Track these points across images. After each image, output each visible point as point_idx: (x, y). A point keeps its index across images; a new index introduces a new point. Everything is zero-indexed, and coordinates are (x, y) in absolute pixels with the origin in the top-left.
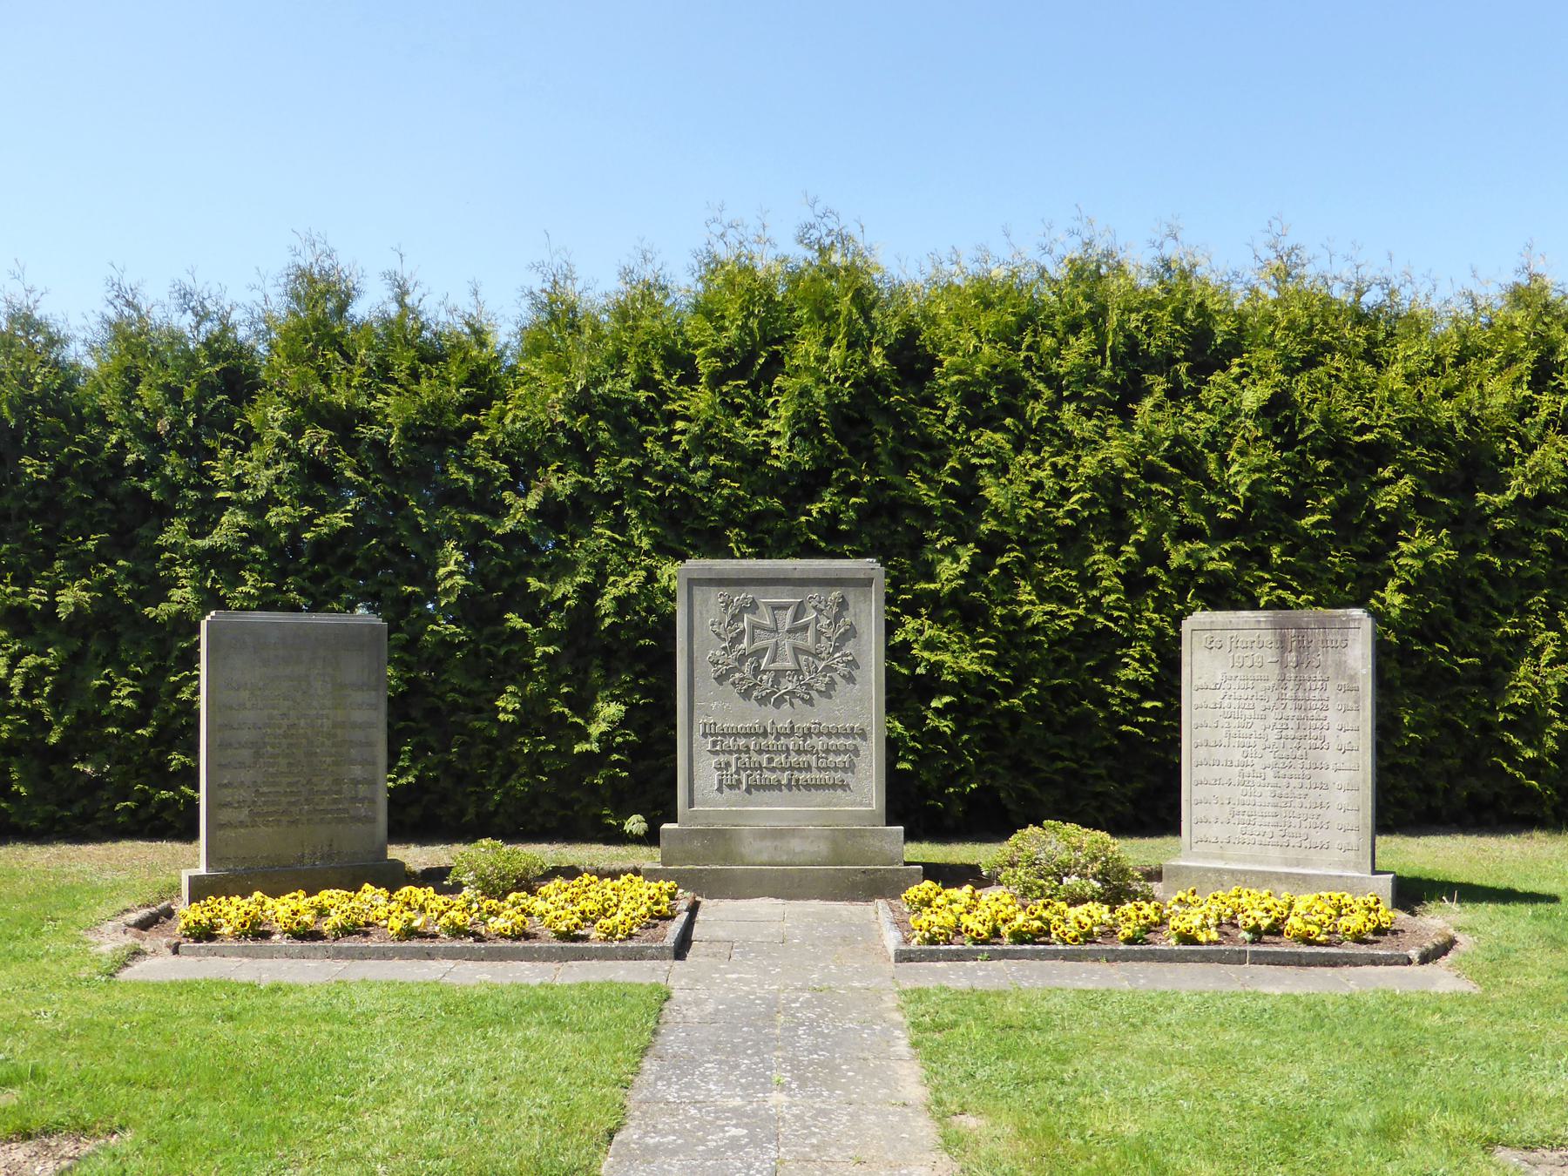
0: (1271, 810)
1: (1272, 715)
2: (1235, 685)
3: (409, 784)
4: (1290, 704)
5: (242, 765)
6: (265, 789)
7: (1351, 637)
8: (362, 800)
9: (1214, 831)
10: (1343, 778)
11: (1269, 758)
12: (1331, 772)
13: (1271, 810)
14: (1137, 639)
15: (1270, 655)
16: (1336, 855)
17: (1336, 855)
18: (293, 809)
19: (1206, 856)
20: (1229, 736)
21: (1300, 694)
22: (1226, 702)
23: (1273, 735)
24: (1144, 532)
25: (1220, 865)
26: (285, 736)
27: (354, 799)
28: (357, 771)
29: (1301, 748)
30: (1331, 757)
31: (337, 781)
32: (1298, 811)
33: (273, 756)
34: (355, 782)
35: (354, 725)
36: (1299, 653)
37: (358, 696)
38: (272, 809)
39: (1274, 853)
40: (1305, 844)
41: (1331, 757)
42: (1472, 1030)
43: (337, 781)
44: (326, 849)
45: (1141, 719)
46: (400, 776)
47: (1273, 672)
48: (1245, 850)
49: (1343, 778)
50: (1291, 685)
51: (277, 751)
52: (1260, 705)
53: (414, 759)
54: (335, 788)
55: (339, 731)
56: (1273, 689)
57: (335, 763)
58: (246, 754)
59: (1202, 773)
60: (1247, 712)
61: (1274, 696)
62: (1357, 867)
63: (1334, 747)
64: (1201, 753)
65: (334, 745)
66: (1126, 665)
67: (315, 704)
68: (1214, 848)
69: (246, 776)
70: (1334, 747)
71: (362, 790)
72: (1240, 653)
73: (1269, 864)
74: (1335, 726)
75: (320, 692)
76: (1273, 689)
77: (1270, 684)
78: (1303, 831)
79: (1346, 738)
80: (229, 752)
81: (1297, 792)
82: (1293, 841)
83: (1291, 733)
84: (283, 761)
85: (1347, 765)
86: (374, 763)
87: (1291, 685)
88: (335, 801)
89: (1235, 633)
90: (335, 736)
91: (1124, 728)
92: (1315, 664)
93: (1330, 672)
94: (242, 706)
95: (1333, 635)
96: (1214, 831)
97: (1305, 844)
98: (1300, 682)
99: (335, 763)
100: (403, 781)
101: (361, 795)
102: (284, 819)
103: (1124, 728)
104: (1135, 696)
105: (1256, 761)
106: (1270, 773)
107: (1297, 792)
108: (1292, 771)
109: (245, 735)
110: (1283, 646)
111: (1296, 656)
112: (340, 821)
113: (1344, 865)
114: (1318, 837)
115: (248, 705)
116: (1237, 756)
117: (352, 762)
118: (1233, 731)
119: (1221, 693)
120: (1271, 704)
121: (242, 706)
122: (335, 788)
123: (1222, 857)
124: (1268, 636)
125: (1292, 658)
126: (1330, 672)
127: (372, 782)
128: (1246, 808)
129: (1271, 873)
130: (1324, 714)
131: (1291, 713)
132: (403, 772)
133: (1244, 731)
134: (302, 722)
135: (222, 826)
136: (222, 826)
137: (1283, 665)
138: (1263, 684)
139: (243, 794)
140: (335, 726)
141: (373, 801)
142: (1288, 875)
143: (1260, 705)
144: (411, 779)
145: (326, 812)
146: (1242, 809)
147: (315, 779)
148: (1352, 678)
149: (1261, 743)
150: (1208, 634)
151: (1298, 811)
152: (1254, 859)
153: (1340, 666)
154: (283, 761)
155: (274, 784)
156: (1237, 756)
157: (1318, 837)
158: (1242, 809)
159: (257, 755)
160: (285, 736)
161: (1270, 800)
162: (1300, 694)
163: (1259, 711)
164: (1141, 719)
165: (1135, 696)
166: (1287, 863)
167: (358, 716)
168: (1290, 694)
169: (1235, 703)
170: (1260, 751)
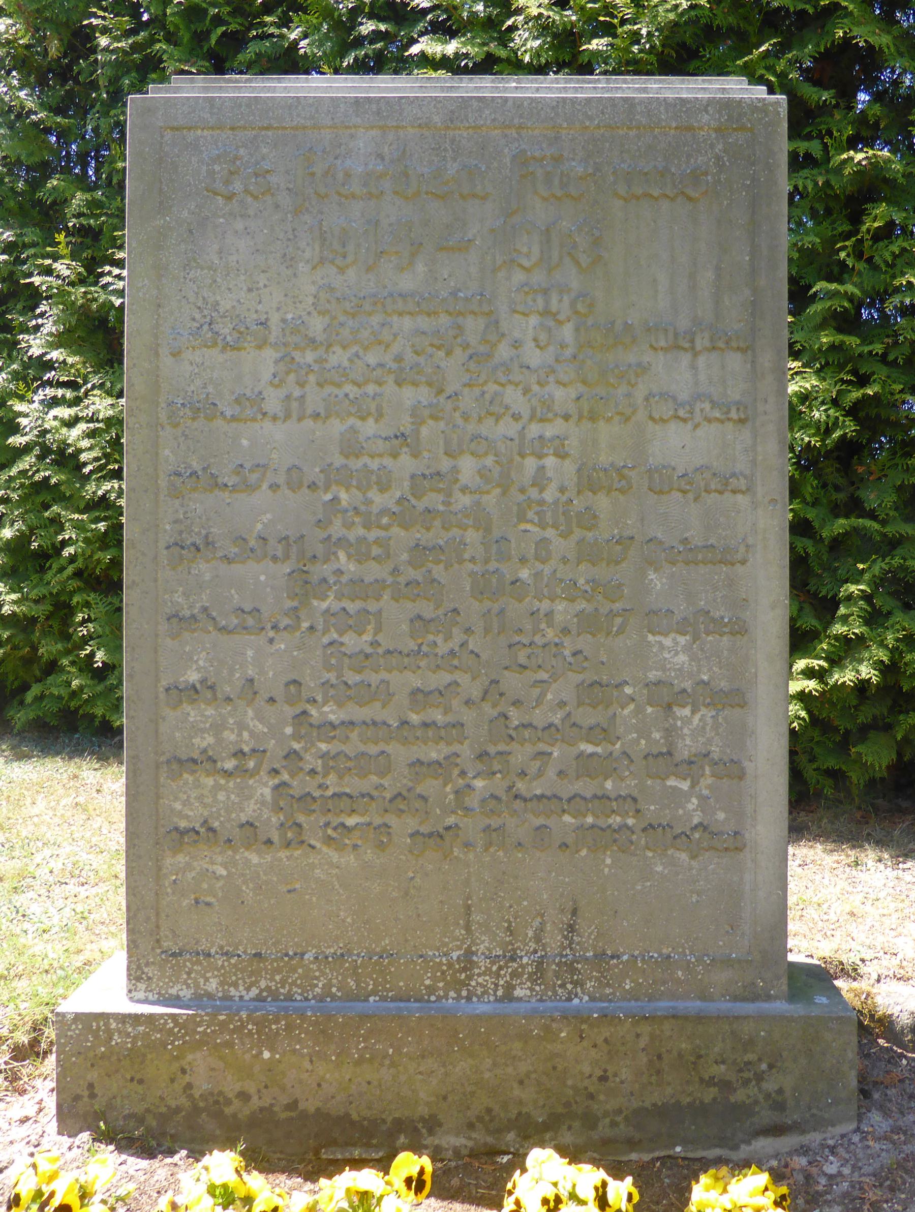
3: (862, 686)
5: (251, 620)
6: (332, 713)
8: (690, 767)
18: (429, 786)
26: (403, 516)
27: (665, 760)
28: (674, 653)
31: (597, 692)
33: (359, 588)
34: (666, 697)
35: (661, 482)
37: (677, 375)
38: (353, 785)
42: (276, 440)
43: (597, 692)
44: (554, 940)
46: (835, 661)
51: (374, 571)
53: (875, 618)
54: (588, 717)
55: (602, 503)
57: (589, 623)
58: (264, 578)
65: (588, 554)
67: (513, 397)
69: (265, 659)
71: (693, 726)
75: (534, 357)
80: (204, 569)
84: (397, 614)
86: (739, 629)
88: (587, 766)
90: (589, 519)
94: (250, 406)
99: (589, 623)
100: (845, 677)
101: (686, 747)
102: (403, 825)
109: (264, 511)
112: (603, 838)
115: (273, 402)
117: (655, 620)
121: (250, 406)
122: (588, 717)
127: (732, 698)
132: (848, 649)
134: (468, 466)
135: (183, 837)
136: (183, 837)
139: (251, 725)
140: (590, 480)
141: (733, 770)
144: (867, 671)
145: (548, 801)
147: (512, 682)
154: (397, 614)
155: (366, 694)
159: (305, 586)
160: (403, 516)
167: (678, 445)
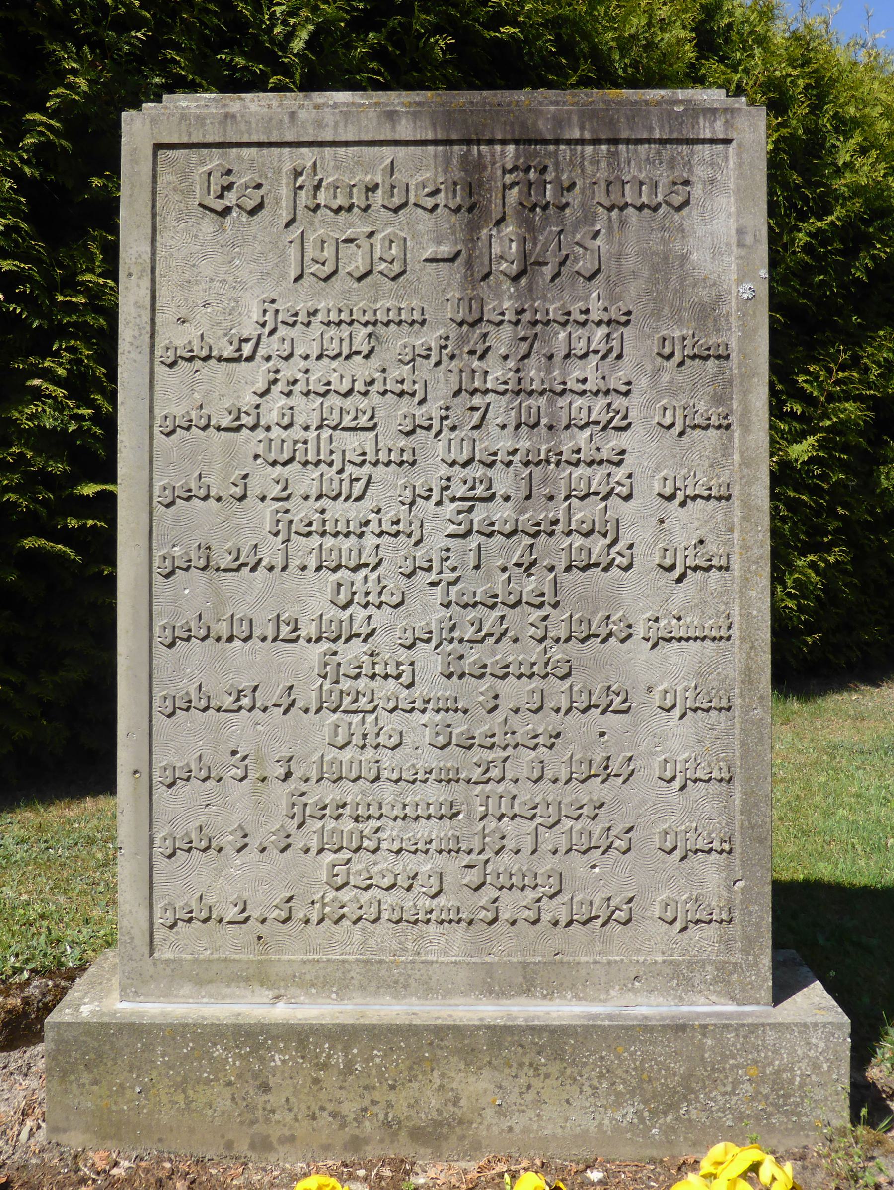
0: (434, 794)
1: (435, 451)
2: (307, 342)
4: (500, 410)
7: (701, 172)
9: (230, 881)
10: (676, 669)
11: (428, 609)
12: (638, 649)
13: (434, 794)
14: (61, 332)
15: (427, 235)
16: (655, 942)
17: (655, 942)
19: (203, 976)
20: (284, 530)
21: (533, 373)
22: (274, 408)
23: (439, 521)
24: (82, 83)
25: (256, 1007)
29: (540, 549)
30: (639, 596)
32: (526, 793)
36: (530, 229)
39: (445, 947)
40: (551, 910)
41: (639, 596)
45: (73, 523)
47: (436, 294)
48: (347, 944)
49: (676, 669)
50: (502, 340)
52: (394, 414)
56: (443, 354)
59: (191, 668)
60: (352, 443)
61: (441, 386)
62: (724, 979)
63: (648, 558)
64: (189, 595)
66: (37, 394)
68: (232, 944)
70: (648, 558)
72: (323, 228)
73: (428, 989)
74: (649, 487)
76: (443, 354)
77: (430, 337)
78: (546, 864)
79: (687, 525)
81: (524, 726)
82: (512, 904)
83: (501, 513)
85: (692, 623)
87: (502, 340)
89: (308, 156)
91: (29, 543)
92: (585, 265)
93: (633, 294)
95: (637, 164)
96: (230, 881)
97: (551, 910)
98: (532, 328)
103: (29, 543)
104: (58, 468)
105: (380, 618)
106: (429, 661)
107: (524, 726)
108: (506, 652)
110: (473, 206)
111: (519, 252)
113: (680, 976)
114: (597, 881)
116: (314, 599)
118: (301, 512)
119: (257, 374)
120: (434, 409)
123: (259, 976)
124: (422, 169)
125: (504, 243)
126: (633, 294)
128: (350, 792)
129: (440, 1031)
130: (613, 442)
131: (503, 443)
133: (337, 510)
137: (478, 274)
138: (399, 341)
142: (499, 1034)
143: (394, 414)
146: (330, 794)
148: (708, 314)
149: (396, 553)
150: (214, 160)
151: (526, 793)
152: (378, 977)
153: (668, 269)
156: (314, 599)
157: (597, 881)
158: (330, 794)
161: (431, 759)
162: (533, 373)
163: (390, 438)
164: (73, 523)
165: (58, 468)
166: (490, 984)
168: (498, 372)
169: (307, 410)
170: (394, 584)
